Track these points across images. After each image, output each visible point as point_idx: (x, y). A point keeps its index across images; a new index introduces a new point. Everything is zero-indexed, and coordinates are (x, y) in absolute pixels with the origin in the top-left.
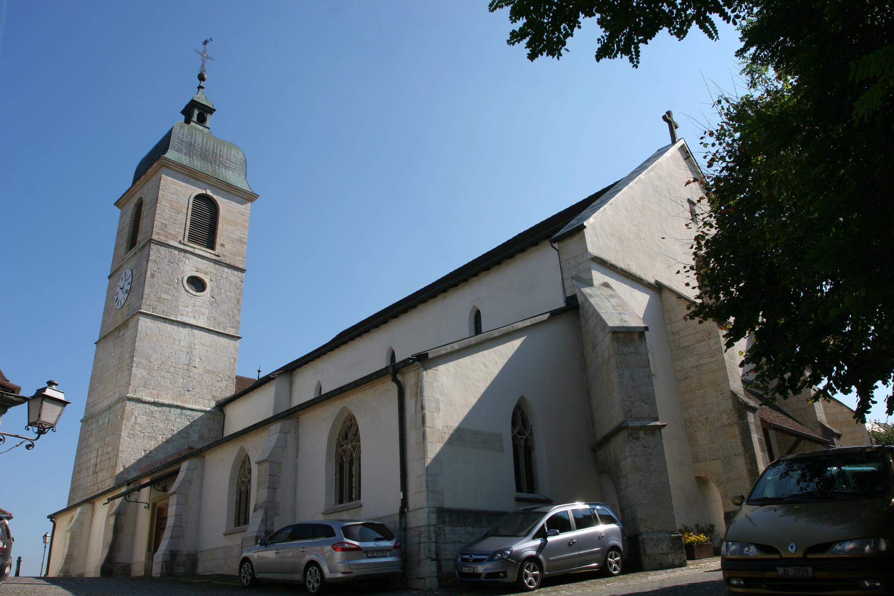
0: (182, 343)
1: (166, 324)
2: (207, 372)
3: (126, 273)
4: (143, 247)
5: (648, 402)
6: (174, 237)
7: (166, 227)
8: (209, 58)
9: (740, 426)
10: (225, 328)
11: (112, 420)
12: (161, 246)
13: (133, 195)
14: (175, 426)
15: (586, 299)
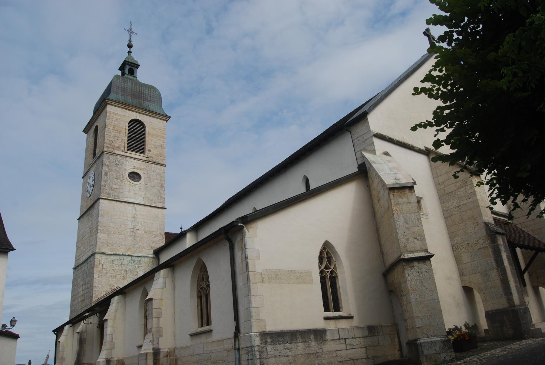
3: (91, 174)
5: (419, 238)
6: (119, 148)
8: (134, 33)
9: (492, 248)
15: (371, 165)
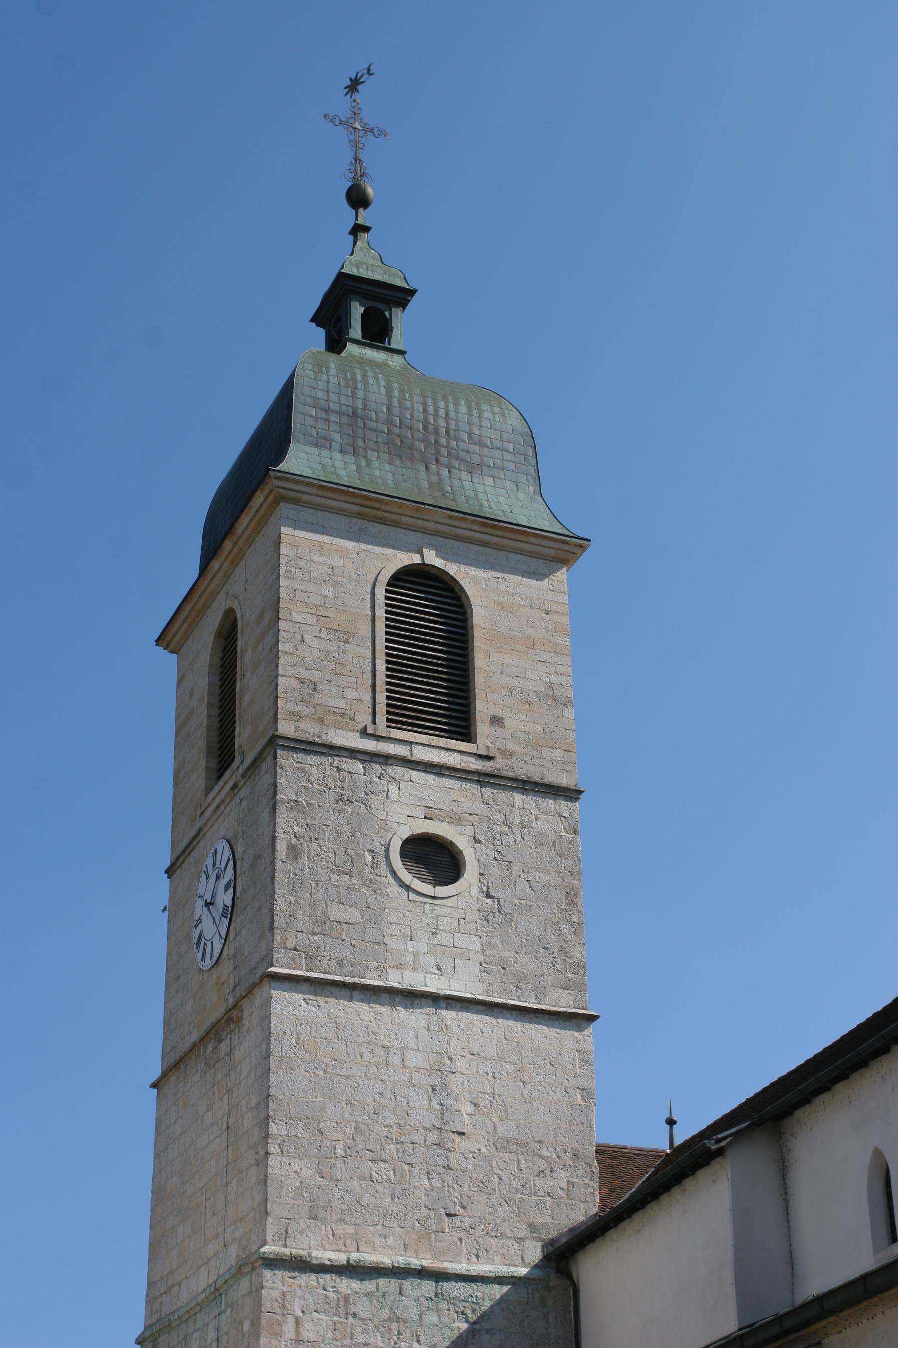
0: (414, 1059)
2: (502, 1145)
6: (344, 719)
7: (315, 690)
10: (539, 991)
11: (227, 1333)
13: (207, 606)
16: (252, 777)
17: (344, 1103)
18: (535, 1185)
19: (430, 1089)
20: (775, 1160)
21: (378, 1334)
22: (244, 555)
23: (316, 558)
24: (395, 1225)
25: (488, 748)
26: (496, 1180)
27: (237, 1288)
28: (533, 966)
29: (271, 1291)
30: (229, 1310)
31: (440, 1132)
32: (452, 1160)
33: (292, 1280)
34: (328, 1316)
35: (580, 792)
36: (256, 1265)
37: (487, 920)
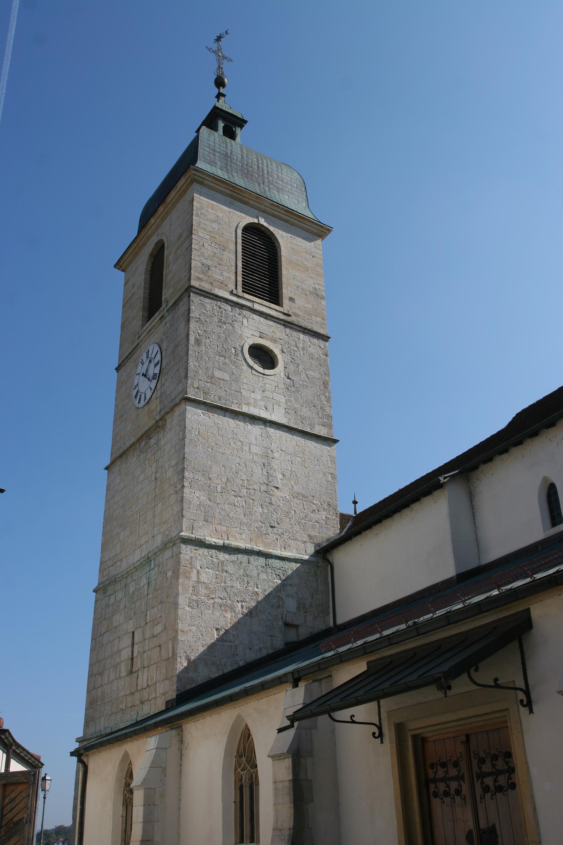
0: (255, 449)
1: (226, 419)
2: (296, 496)
4: (176, 303)
6: (222, 285)
7: (209, 269)
8: (226, 58)
10: (312, 426)
11: (155, 580)
12: (205, 296)
13: (144, 244)
14: (259, 586)
16: (173, 310)
17: (221, 466)
18: (311, 517)
19: (262, 465)
20: (467, 492)
21: (238, 582)
22: (170, 213)
23: (210, 210)
24: (246, 529)
25: (288, 310)
26: (293, 512)
27: (162, 556)
28: (309, 414)
29: (185, 556)
30: (157, 568)
31: (267, 486)
32: (273, 500)
33: (195, 551)
34: (213, 571)
35: (329, 338)
36: (176, 542)
37: (288, 389)
